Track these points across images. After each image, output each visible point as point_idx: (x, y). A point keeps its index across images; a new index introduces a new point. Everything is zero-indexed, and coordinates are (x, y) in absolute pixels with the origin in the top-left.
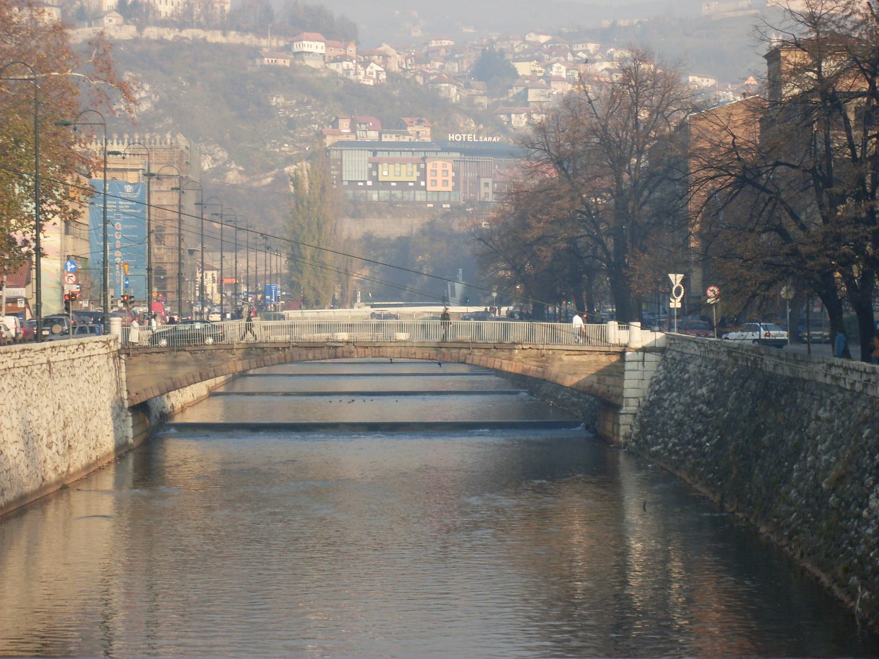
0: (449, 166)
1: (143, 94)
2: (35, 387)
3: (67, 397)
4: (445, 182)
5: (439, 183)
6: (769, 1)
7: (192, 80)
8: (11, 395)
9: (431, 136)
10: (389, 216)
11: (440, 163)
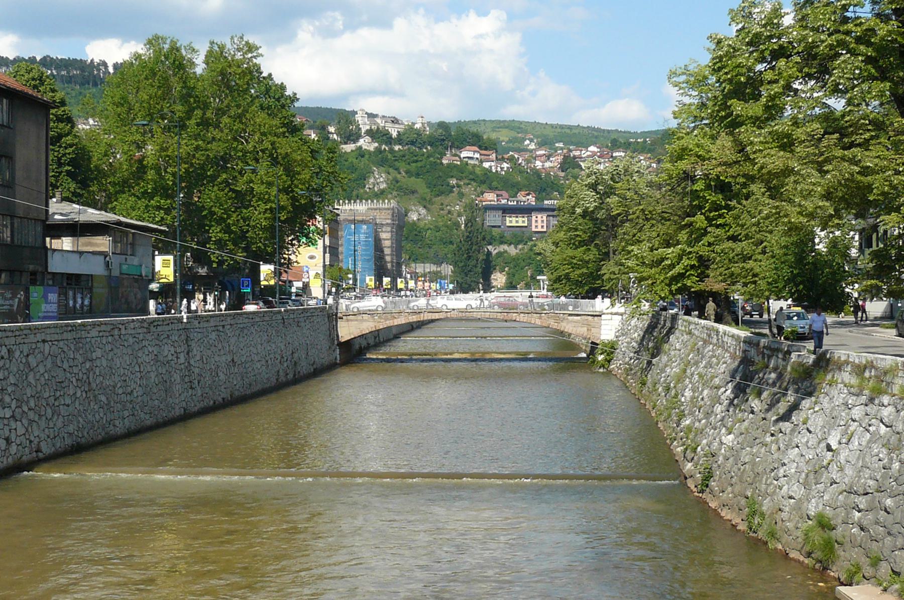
0: (545, 218)
1: (382, 180)
2: (274, 332)
3: (295, 337)
4: (542, 227)
5: (540, 227)
6: (1, 460)
7: (781, 488)
8: (257, 336)
9: (535, 202)
10: (27, 58)
11: (539, 216)
